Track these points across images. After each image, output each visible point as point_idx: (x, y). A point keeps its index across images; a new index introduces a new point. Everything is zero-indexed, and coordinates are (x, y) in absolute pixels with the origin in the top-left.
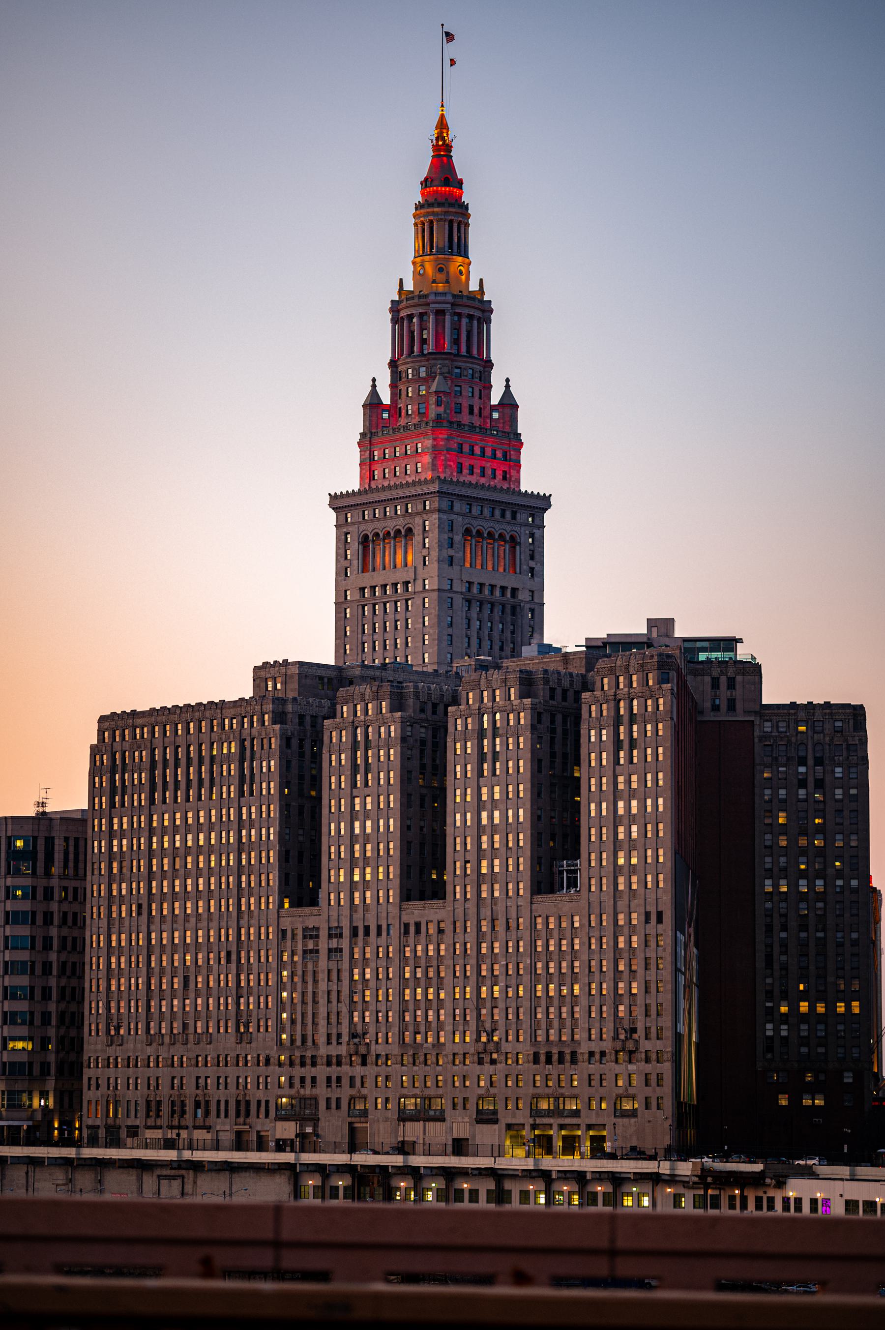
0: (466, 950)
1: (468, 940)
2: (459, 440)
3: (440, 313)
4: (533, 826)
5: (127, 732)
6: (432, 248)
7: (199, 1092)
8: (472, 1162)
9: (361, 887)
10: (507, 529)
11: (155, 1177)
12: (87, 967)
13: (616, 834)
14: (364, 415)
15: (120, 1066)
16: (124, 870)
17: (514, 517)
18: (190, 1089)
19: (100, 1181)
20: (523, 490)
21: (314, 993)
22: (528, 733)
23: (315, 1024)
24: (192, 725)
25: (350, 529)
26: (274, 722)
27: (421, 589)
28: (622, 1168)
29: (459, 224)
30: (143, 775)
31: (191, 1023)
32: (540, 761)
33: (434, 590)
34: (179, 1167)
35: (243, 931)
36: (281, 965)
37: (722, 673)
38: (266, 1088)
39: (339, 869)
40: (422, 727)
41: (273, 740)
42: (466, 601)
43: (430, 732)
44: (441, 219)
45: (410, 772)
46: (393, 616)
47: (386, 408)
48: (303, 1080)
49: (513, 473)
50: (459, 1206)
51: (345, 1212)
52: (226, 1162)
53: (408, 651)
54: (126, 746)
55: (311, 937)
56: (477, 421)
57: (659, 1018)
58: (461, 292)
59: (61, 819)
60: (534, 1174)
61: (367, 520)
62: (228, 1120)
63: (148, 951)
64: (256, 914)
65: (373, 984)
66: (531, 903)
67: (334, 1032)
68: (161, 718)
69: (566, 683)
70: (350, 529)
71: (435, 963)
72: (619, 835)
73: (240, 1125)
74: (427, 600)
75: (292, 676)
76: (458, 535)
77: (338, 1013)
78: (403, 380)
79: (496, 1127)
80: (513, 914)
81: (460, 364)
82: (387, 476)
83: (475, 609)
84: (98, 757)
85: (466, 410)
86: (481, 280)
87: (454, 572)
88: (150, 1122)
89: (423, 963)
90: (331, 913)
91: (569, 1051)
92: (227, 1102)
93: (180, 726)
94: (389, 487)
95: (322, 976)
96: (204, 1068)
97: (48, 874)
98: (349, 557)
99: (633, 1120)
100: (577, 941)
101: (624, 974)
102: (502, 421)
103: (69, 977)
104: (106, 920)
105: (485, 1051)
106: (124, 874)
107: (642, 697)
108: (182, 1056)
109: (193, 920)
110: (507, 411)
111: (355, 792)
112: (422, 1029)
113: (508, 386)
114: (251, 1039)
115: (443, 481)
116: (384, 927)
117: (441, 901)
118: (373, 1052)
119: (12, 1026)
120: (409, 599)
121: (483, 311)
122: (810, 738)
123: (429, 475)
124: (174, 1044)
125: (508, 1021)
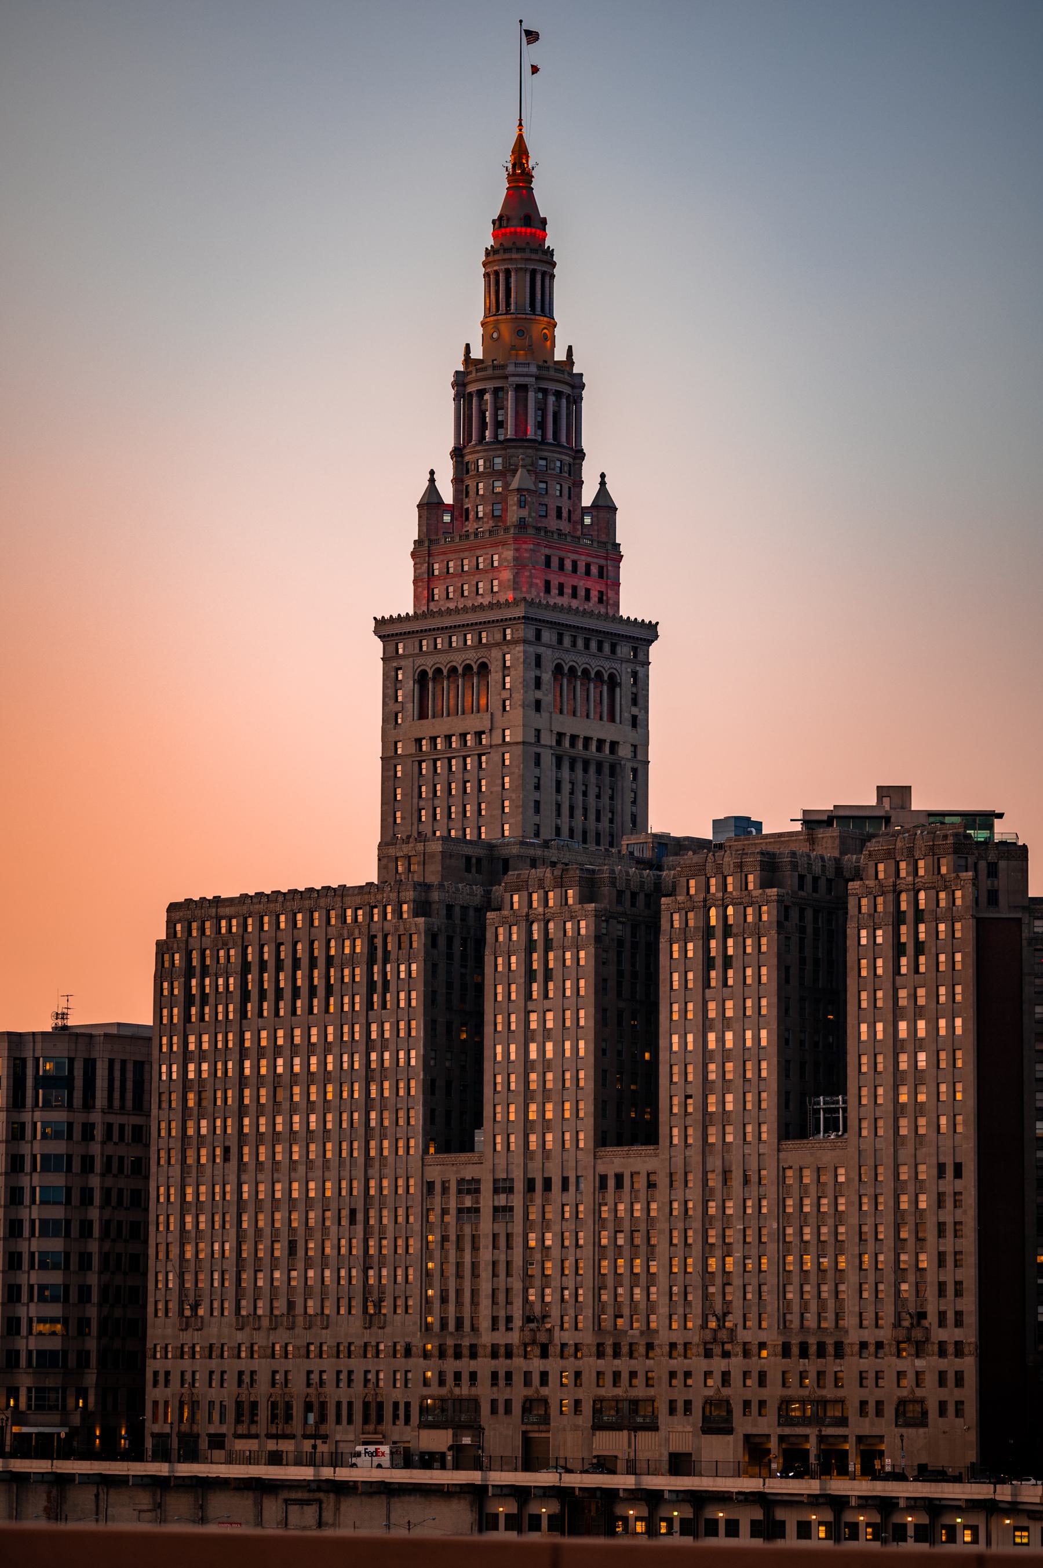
0: (686, 1210)
1: (691, 1197)
2: (547, 551)
4: (780, 1053)
5: (208, 924)
6: (508, 304)
7: (311, 1390)
8: (731, 1485)
9: (539, 1128)
10: (607, 666)
11: (280, 1501)
12: (152, 1228)
13: (896, 1063)
14: (420, 517)
15: (197, 1356)
16: (204, 1103)
17: (613, 651)
18: (298, 1386)
19: (201, 1507)
21: (473, 1263)
22: (774, 932)
23: (475, 1303)
24: (299, 916)
25: (403, 663)
26: (416, 914)
27: (500, 742)
28: (942, 1492)
29: (544, 274)
30: (231, 980)
31: (299, 1301)
32: (787, 968)
33: (517, 743)
34: (319, 1489)
35: (372, 1183)
36: (427, 1226)
37: (980, 857)
38: (406, 1386)
39: (508, 1105)
40: (619, 922)
41: (415, 937)
43: (629, 930)
44: (521, 269)
45: (605, 980)
46: (461, 776)
47: (450, 508)
48: (457, 1376)
49: (611, 594)
50: (711, 1542)
51: (503, 1547)
52: (383, 1482)
53: (482, 821)
54: (207, 942)
56: (565, 526)
57: (958, 1300)
58: (545, 362)
59: (106, 1035)
60: (821, 1500)
61: (426, 652)
62: (351, 1428)
63: (238, 1208)
64: (391, 1160)
65: (556, 1253)
66: (779, 1151)
67: (502, 1314)
68: (257, 906)
69: (817, 869)
70: (403, 663)
71: (643, 1227)
72: (901, 1064)
73: (369, 1433)
74: (507, 756)
75: (433, 855)
77: (507, 1290)
78: (471, 473)
79: (730, 1438)
80: (753, 1165)
81: (546, 454)
82: (451, 595)
84: (167, 957)
85: (553, 513)
86: (570, 348)
87: (541, 721)
88: (242, 1429)
89: (626, 1226)
90: (496, 1161)
91: (832, 1342)
92: (350, 1404)
93: (282, 918)
94: (457, 611)
95: (485, 1242)
96: (318, 1360)
97: (88, 1104)
98: (400, 699)
99: (922, 1431)
100: (842, 1200)
101: (909, 1242)
102: (596, 528)
104: (178, 1167)
105: (715, 1340)
106: (205, 1108)
107: (933, 888)
108: (287, 1345)
109: (302, 1169)
110: (603, 514)
111: (531, 1006)
112: (626, 1311)
113: (603, 484)
114: (385, 1323)
115: (531, 604)
116: (572, 1180)
117: (652, 1147)
118: (557, 1341)
119: (40, 1304)
120: (484, 754)
121: (573, 387)
123: (510, 595)
124: (275, 1329)
125: (746, 1302)
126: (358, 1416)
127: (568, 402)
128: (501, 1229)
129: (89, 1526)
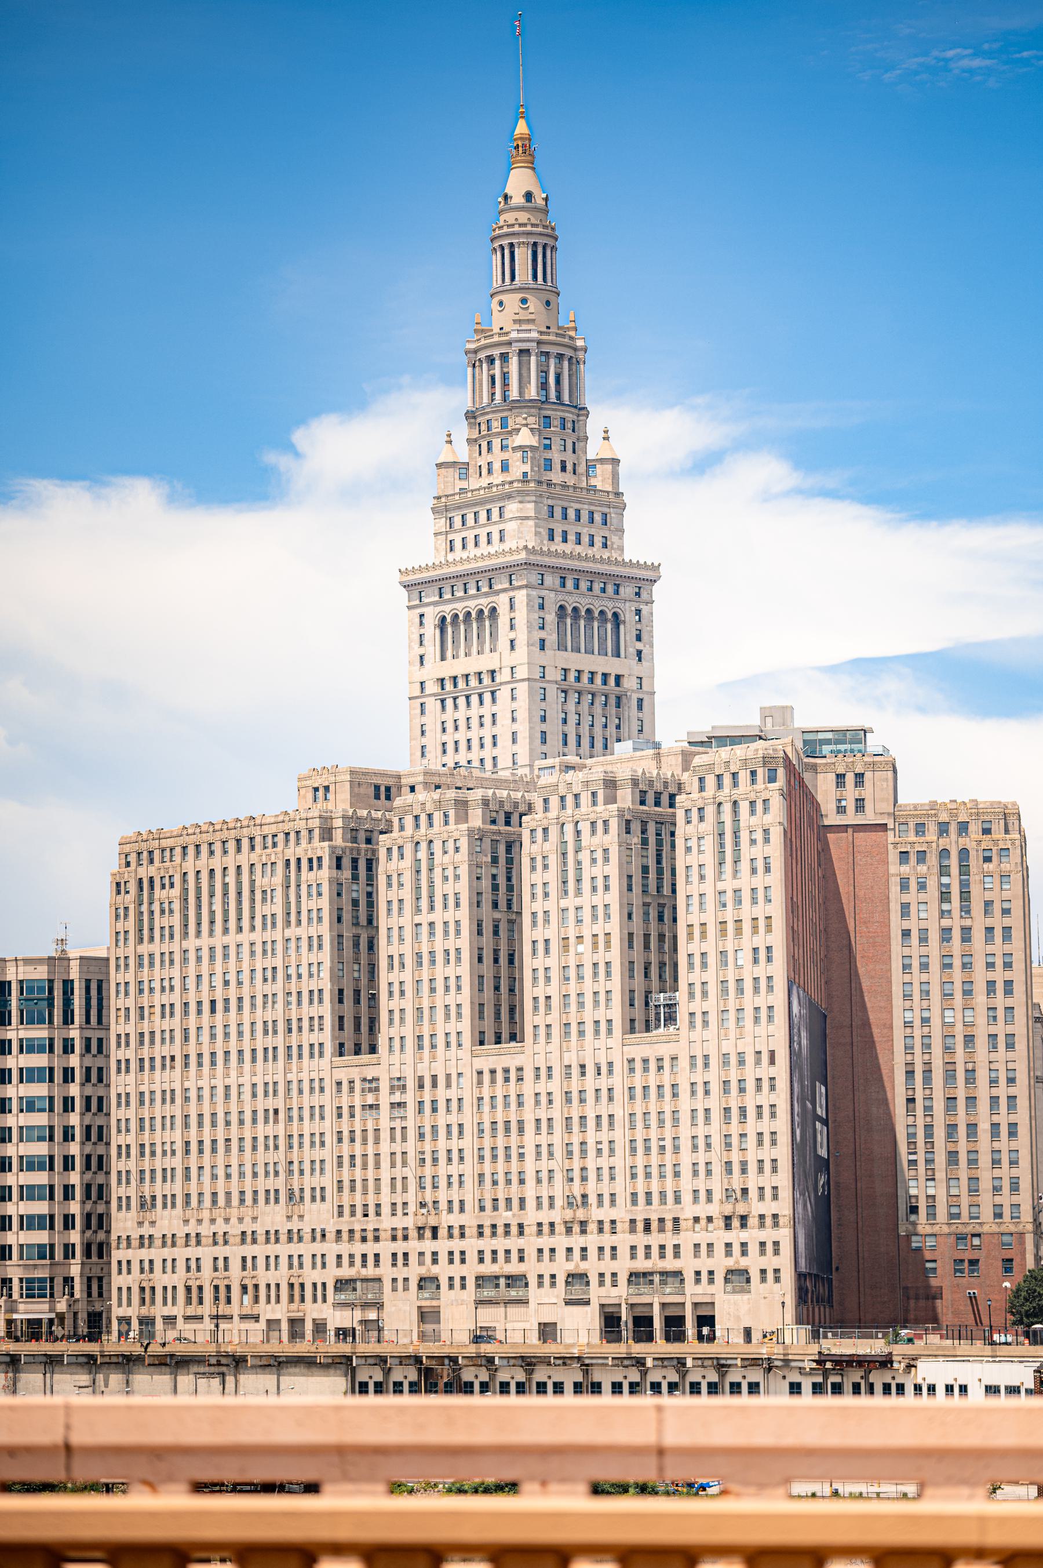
2: (550, 502)
3: (524, 353)
20: (627, 560)
42: (562, 691)
55: (370, 1090)
76: (550, 614)
83: (573, 697)
85: (557, 466)
97: (68, 1018)
103: (95, 1144)
122: (953, 843)
126: (159, 1292)
127: (570, 364)
128: (398, 1124)
129: (39, 1399)
